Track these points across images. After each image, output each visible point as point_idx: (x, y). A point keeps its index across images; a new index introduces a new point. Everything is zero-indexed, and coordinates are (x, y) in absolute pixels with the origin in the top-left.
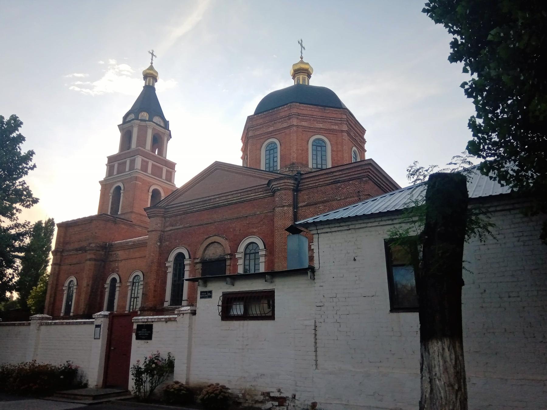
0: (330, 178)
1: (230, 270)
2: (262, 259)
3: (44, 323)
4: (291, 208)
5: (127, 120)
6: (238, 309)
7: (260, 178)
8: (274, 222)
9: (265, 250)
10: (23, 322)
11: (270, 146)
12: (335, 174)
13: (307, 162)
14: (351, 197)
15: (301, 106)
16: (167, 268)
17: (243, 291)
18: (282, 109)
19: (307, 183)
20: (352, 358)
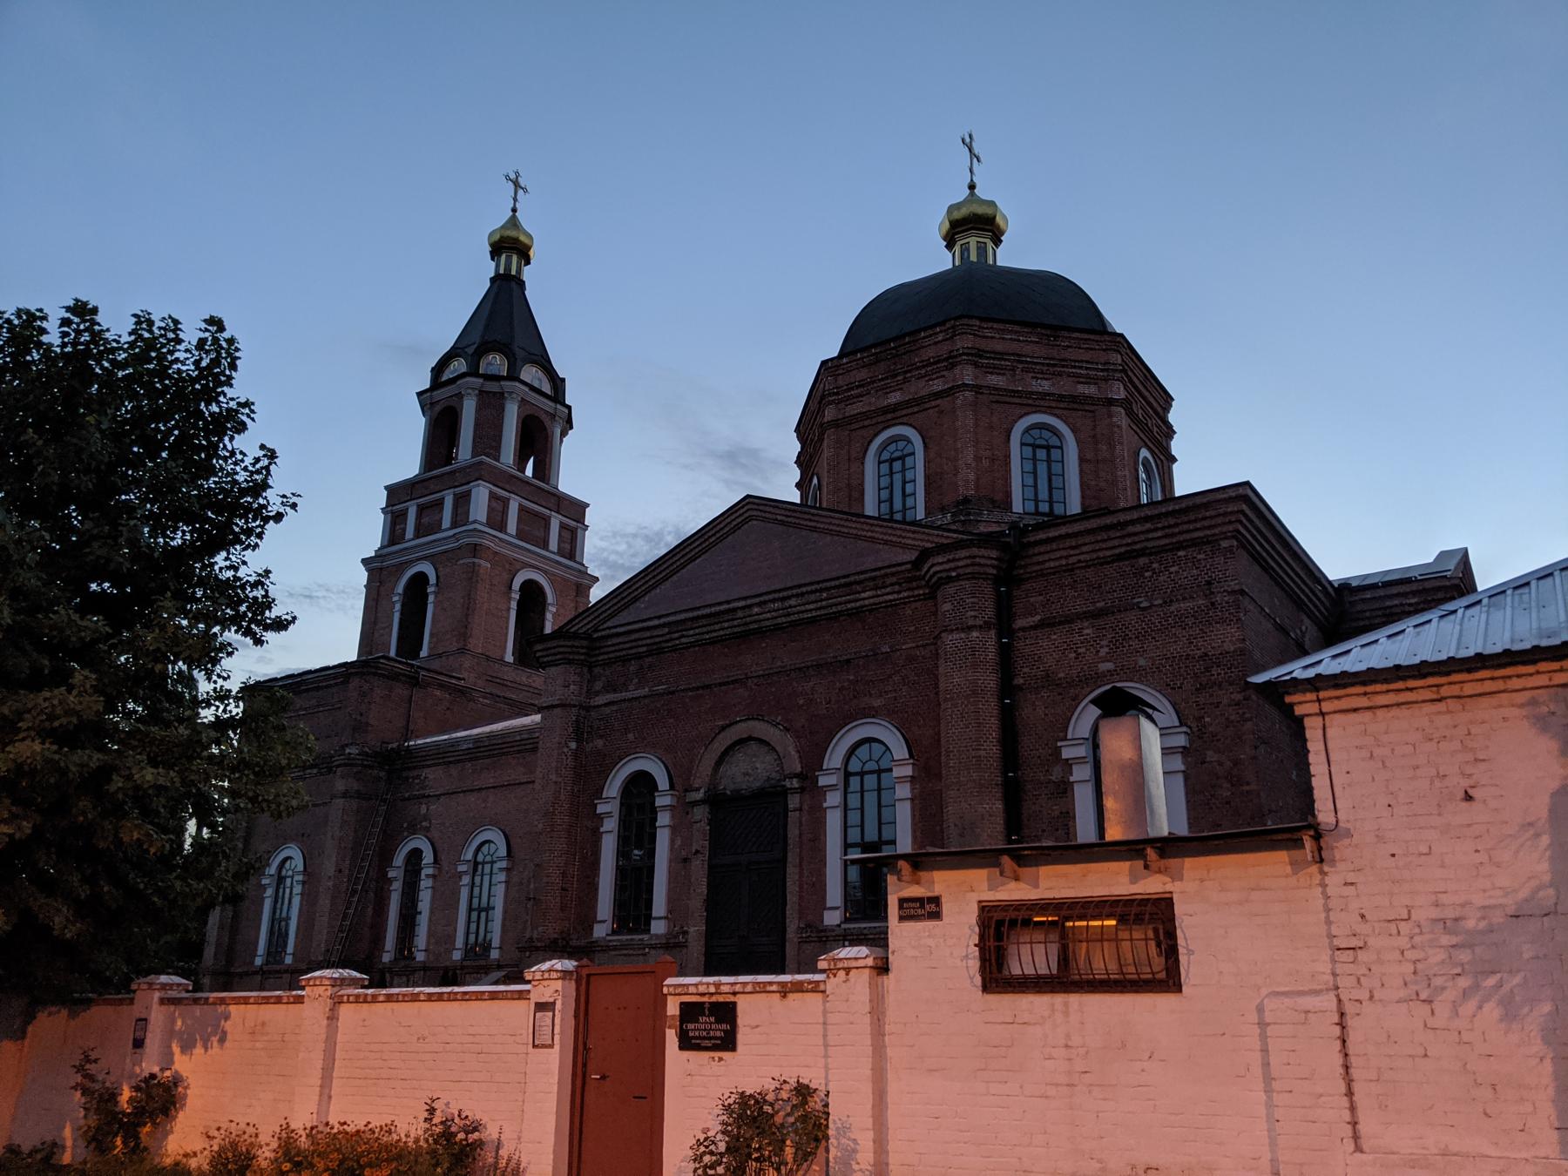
0: (1116, 543)
1: (801, 822)
2: (904, 791)
3: (349, 996)
4: (993, 633)
5: (444, 378)
6: (1031, 957)
7: (886, 542)
8: (936, 677)
9: (911, 761)
10: (278, 993)
11: (892, 447)
12: (1131, 529)
13: (1008, 495)
14: (1184, 599)
15: (987, 328)
16: (600, 818)
17: (1054, 899)
18: (927, 337)
19: (1041, 558)
20: (1486, 1114)
